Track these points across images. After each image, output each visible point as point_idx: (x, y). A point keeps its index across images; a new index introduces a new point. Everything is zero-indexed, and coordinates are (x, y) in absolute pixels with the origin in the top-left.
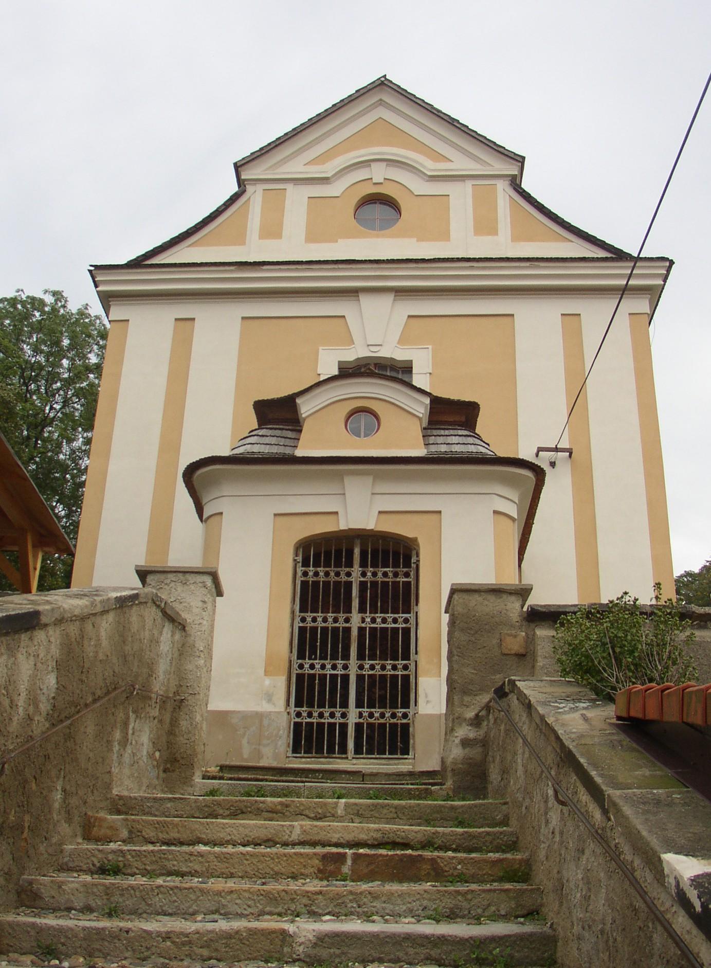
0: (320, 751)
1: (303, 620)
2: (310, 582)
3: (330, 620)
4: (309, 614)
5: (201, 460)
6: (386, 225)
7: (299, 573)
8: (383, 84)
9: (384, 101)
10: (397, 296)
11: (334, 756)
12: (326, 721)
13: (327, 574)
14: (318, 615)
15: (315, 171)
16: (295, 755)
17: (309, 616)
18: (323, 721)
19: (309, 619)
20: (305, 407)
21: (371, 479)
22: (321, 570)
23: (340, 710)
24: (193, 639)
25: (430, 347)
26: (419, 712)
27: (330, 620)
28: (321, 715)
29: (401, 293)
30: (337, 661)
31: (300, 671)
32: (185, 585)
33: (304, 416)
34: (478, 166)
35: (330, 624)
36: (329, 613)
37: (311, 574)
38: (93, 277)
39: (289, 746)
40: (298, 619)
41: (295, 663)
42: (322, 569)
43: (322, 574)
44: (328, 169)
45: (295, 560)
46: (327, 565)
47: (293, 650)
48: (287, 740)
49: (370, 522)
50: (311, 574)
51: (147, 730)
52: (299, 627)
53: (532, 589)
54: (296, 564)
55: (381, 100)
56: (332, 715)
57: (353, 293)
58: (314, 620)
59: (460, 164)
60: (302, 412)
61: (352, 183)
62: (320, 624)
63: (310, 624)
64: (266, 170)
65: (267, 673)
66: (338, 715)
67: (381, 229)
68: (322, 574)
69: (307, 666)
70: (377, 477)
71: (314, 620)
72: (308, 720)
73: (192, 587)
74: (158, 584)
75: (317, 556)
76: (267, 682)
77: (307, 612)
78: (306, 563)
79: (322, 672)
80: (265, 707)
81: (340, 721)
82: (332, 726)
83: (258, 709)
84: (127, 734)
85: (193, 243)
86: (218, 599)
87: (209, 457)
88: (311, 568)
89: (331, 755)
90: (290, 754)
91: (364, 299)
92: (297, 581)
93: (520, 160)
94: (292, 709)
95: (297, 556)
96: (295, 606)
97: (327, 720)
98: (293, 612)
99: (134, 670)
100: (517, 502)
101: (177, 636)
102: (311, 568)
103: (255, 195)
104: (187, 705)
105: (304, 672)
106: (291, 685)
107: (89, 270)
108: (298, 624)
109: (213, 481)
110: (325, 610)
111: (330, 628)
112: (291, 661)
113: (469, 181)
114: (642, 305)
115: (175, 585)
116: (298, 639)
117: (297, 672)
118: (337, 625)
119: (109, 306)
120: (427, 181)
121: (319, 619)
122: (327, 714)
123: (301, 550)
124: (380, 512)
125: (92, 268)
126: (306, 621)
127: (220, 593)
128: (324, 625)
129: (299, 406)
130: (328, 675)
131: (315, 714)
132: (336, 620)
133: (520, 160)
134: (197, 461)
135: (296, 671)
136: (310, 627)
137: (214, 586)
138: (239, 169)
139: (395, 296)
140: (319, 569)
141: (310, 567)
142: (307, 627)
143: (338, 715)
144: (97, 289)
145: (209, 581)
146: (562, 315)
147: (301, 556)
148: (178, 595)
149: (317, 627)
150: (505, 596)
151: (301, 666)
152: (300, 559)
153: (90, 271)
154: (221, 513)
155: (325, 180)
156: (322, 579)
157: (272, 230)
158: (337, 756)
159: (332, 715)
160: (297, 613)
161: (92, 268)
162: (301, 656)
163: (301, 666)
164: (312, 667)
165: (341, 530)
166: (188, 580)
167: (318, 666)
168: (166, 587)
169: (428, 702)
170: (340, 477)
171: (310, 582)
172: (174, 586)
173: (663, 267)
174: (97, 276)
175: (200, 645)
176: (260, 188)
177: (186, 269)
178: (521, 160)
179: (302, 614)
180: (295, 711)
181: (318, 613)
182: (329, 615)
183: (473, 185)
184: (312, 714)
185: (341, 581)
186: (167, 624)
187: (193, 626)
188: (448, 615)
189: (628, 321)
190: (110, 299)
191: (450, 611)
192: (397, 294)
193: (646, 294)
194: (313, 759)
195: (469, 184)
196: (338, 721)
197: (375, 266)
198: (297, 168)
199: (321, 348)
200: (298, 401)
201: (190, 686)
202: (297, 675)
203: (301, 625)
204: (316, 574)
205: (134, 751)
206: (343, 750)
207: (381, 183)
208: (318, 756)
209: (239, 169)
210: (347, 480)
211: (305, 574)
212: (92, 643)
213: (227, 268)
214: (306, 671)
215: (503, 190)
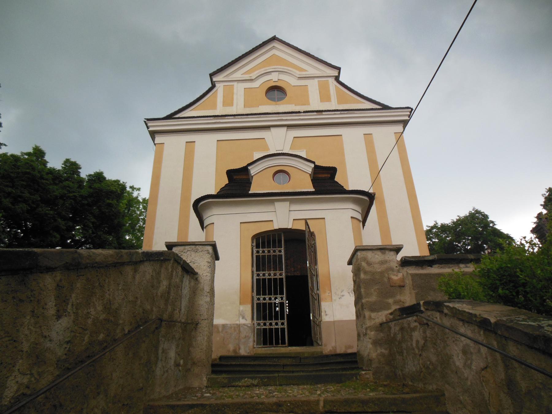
0: (271, 343)
1: (258, 275)
2: (261, 256)
3: (272, 275)
4: (261, 272)
5: (202, 197)
6: (280, 99)
7: (255, 252)
8: (274, 39)
9: (276, 47)
10: (289, 128)
11: (279, 346)
12: (274, 327)
13: (269, 252)
14: (266, 272)
15: (247, 77)
16: (258, 346)
17: (261, 273)
18: (272, 327)
19: (261, 275)
20: (253, 170)
21: (288, 203)
22: (266, 250)
23: (281, 321)
24: (202, 285)
25: (305, 150)
26: (323, 321)
27: (272, 275)
28: (271, 324)
29: (289, 126)
30: (277, 296)
31: (258, 302)
32: (196, 253)
33: (252, 175)
34: (320, 73)
35: (272, 277)
36: (271, 271)
37: (261, 252)
38: (146, 124)
39: (255, 342)
40: (255, 275)
41: (255, 298)
42: (266, 249)
43: (266, 252)
44: (254, 75)
45: (252, 245)
46: (269, 247)
47: (254, 291)
48: (253, 339)
49: (289, 225)
50: (261, 252)
51: (174, 347)
52: (256, 279)
53: (402, 248)
54: (253, 247)
55: (274, 46)
56: (277, 324)
57: (268, 127)
58: (264, 275)
59: (311, 71)
60: (251, 173)
61: (263, 82)
62: (267, 277)
63: (261, 277)
64: (224, 77)
65: (240, 304)
66: (280, 324)
67: (278, 101)
68: (266, 252)
69: (261, 299)
70: (292, 202)
71: (264, 275)
72: (264, 327)
73: (201, 253)
74: (180, 252)
75: (263, 243)
76: (242, 308)
77: (260, 271)
78: (258, 246)
79: (269, 301)
80: (242, 321)
81: (281, 327)
82: (277, 330)
83: (238, 322)
84: (157, 354)
85: (192, 110)
86: (216, 262)
87: (206, 195)
88: (261, 249)
89: (277, 346)
90: (255, 346)
91: (273, 129)
92: (254, 256)
93: (339, 69)
94: (255, 321)
95: (253, 243)
96: (253, 268)
97: (274, 327)
98: (253, 272)
99: (162, 307)
100: (361, 213)
101: (193, 284)
102: (261, 249)
103: (220, 87)
104: (200, 327)
105: (260, 302)
106: (254, 310)
107: (144, 121)
108: (255, 277)
109: (208, 206)
110: (269, 270)
111: (272, 279)
112: (253, 297)
113: (316, 79)
114: (399, 128)
115: (191, 253)
116: (256, 285)
117: (257, 302)
118: (276, 277)
119: (155, 138)
120: (297, 80)
121: (267, 275)
122: (274, 324)
123: (255, 240)
124: (294, 220)
125: (146, 120)
126: (260, 275)
127: (217, 258)
128: (269, 277)
129: (250, 171)
130: (262, 304)
131: (268, 324)
132: (275, 275)
133: (339, 69)
134: (198, 199)
135: (255, 302)
136: (262, 279)
137: (214, 253)
138: (212, 77)
139: (287, 129)
140: (264, 249)
141: (260, 248)
142: (260, 279)
143: (280, 324)
144: (148, 129)
145: (210, 249)
146: (364, 134)
147: (255, 243)
148: (193, 259)
149: (266, 279)
150: (387, 252)
151: (259, 299)
152: (254, 244)
153: (145, 122)
154: (213, 223)
155: (251, 80)
156: (266, 254)
157: (228, 102)
158: (281, 346)
159: (277, 324)
160: (255, 272)
161: (146, 120)
162: (258, 293)
163: (259, 299)
164: (264, 299)
165: (275, 229)
166: (198, 250)
167: (267, 299)
168: (185, 254)
169: (326, 315)
170: (273, 202)
171: (261, 256)
172: (190, 254)
173: (409, 111)
174: (148, 123)
175: (207, 289)
176: (222, 84)
177: (189, 119)
178: (339, 69)
179: (258, 272)
180: (257, 323)
181: (266, 271)
182: (271, 272)
183: (318, 81)
184: (266, 324)
185: (277, 255)
186: (185, 276)
187: (203, 277)
188: (351, 266)
189: (394, 136)
190: (155, 134)
191: (353, 263)
192: (288, 128)
193: (401, 124)
194: (268, 348)
195: (316, 80)
196: (280, 327)
197: (277, 115)
198: (238, 75)
199: (254, 153)
200: (249, 168)
201: (202, 314)
202: (257, 304)
203: (257, 278)
204: (263, 252)
205: (164, 365)
206: (283, 342)
207: (277, 81)
208: (270, 346)
209: (212, 77)
210: (277, 204)
211: (258, 252)
212: (120, 288)
213: (209, 118)
214: (262, 301)
215: (332, 81)
